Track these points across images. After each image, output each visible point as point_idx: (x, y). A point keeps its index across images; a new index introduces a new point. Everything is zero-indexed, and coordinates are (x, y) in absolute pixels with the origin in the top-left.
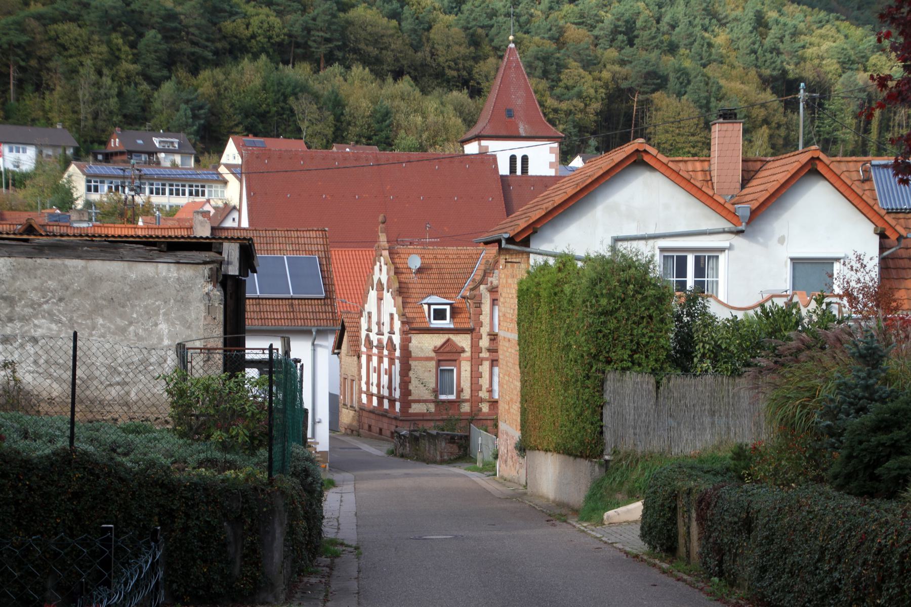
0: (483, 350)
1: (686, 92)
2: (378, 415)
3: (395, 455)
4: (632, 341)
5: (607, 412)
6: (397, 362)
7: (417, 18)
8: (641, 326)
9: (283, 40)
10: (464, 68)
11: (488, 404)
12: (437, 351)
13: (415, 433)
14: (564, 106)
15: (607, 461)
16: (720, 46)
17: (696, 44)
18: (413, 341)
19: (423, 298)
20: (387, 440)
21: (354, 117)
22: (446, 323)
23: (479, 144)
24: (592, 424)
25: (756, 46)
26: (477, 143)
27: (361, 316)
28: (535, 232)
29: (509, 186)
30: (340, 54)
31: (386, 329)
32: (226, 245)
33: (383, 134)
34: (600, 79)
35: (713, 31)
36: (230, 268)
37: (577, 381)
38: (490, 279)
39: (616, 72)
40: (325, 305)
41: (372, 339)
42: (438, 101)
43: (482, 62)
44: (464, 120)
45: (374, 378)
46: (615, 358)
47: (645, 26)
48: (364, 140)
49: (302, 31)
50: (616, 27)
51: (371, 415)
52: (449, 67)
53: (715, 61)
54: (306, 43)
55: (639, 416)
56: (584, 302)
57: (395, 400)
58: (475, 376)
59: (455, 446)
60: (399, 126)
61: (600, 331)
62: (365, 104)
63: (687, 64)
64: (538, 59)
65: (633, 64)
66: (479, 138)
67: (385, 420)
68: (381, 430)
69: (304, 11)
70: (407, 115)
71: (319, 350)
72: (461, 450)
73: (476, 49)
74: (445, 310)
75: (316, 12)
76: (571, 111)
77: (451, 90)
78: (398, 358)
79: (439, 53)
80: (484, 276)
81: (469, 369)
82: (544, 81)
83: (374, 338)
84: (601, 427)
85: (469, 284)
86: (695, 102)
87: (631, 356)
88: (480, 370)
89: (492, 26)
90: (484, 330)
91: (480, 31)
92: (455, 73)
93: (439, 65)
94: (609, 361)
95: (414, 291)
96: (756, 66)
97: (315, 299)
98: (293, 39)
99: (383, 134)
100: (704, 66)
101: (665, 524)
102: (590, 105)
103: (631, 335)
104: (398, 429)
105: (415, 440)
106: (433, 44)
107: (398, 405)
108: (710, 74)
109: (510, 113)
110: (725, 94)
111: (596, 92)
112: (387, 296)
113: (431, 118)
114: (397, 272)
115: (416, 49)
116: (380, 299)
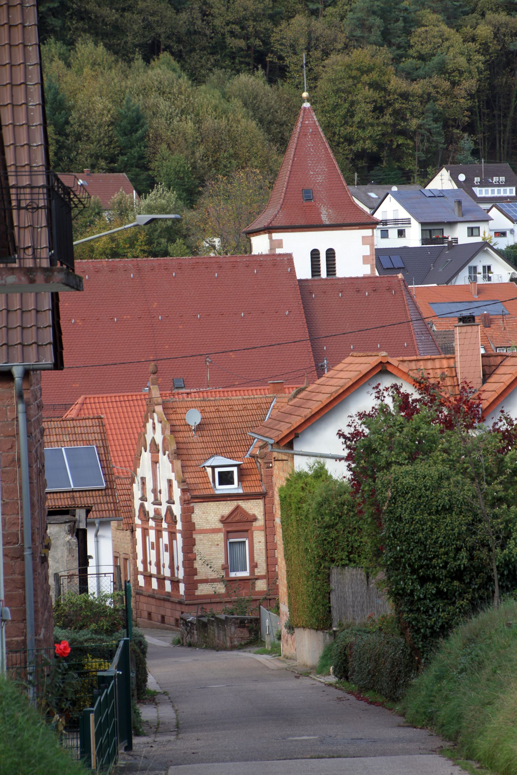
2: (159, 599)
3: (182, 645)
4: (348, 546)
5: (333, 597)
6: (179, 536)
8: (354, 534)
10: (257, 34)
12: (224, 521)
14: (417, 88)
15: (334, 631)
19: (206, 460)
20: (170, 629)
21: (86, 127)
22: (234, 488)
23: (270, 238)
24: (323, 605)
26: (267, 236)
27: (133, 481)
28: (297, 436)
29: (311, 293)
31: (164, 497)
32: (78, 511)
33: (135, 152)
34: (473, 39)
36: (81, 524)
37: (312, 575)
40: (106, 495)
41: (147, 509)
42: (217, 93)
43: (284, 24)
44: (261, 121)
45: (152, 555)
46: (337, 558)
48: (103, 163)
51: (150, 599)
52: (232, 33)
55: (356, 598)
56: (314, 519)
57: (178, 582)
59: (245, 631)
60: (158, 137)
61: (325, 540)
62: (100, 104)
64: (374, 13)
66: (269, 230)
67: (168, 605)
68: (163, 617)
70: (170, 118)
71: (102, 541)
72: (252, 634)
74: (232, 472)
76: (429, 94)
77: (238, 72)
78: (180, 531)
81: (263, 540)
82: (385, 49)
83: (150, 508)
84: (330, 607)
87: (348, 556)
92: (242, 43)
93: (214, 30)
94: (333, 561)
95: (194, 452)
97: (95, 490)
99: (135, 152)
101: (342, 664)
102: (458, 83)
103: (347, 541)
104: (184, 616)
105: (203, 626)
107: (182, 586)
109: (308, 195)
111: (469, 60)
112: (164, 459)
113: (209, 123)
116: (155, 462)
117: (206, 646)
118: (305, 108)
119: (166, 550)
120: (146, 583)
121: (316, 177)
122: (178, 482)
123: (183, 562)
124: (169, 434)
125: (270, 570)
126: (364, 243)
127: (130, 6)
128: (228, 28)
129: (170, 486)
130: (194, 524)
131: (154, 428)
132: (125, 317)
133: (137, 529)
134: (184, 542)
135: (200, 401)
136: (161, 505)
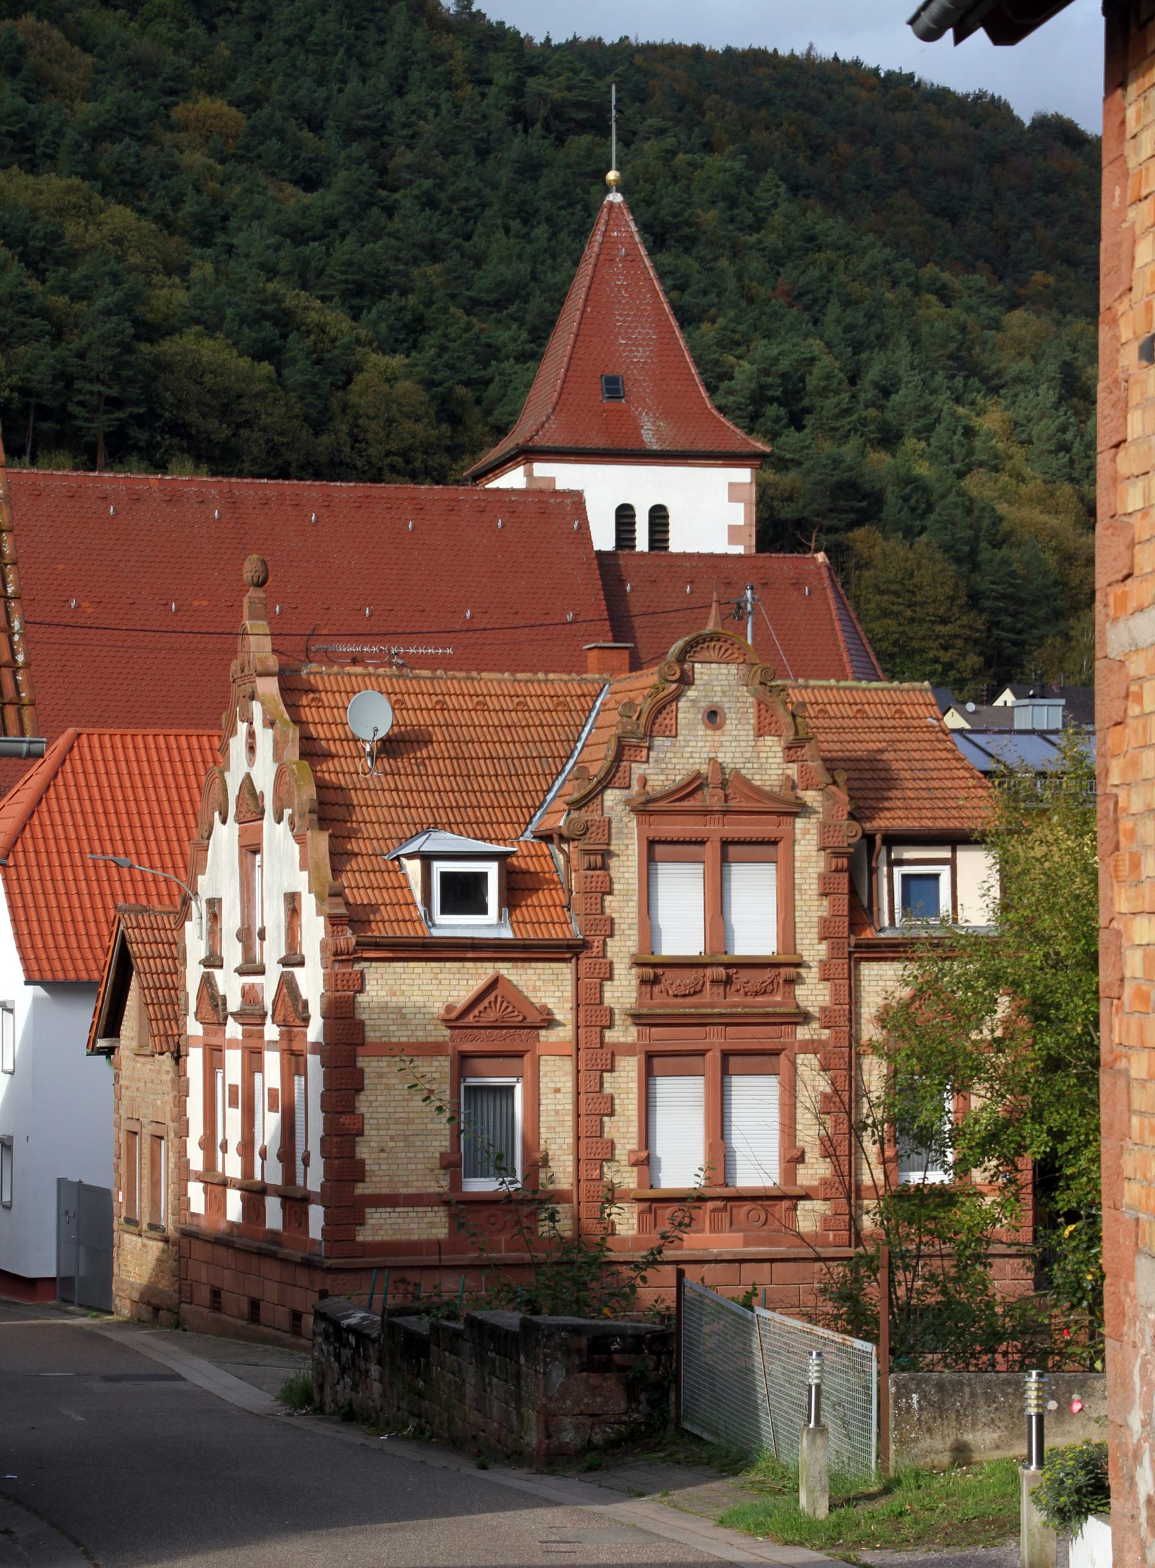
0: (618, 1018)
1: (923, 530)
2: (245, 1251)
3: (320, 1410)
7: (318, 362)
9: (9, 401)
11: (636, 1208)
12: (456, 1020)
13: (411, 1323)
16: (991, 435)
17: (940, 428)
18: (371, 986)
20: (276, 1342)
22: (487, 923)
25: (1069, 436)
27: (185, 915)
29: (622, 583)
30: (140, 435)
31: (272, 951)
35: (973, 403)
38: (638, 769)
39: (768, 485)
45: (231, 1123)
47: (825, 388)
49: (54, 381)
50: (763, 387)
51: (221, 1252)
53: (981, 464)
54: (63, 407)
57: (305, 1199)
58: (593, 1109)
59: (611, 1384)
63: (922, 469)
65: (808, 465)
66: (527, 454)
67: (272, 1269)
68: (255, 1305)
69: (57, 337)
73: (454, 431)
74: (482, 877)
75: (85, 339)
78: (316, 1048)
79: (370, 436)
80: (618, 757)
81: (568, 1084)
83: (230, 985)
85: (564, 787)
86: (947, 548)
88: (608, 1089)
89: (489, 382)
90: (621, 949)
91: (461, 391)
95: (370, 814)
96: (1072, 480)
98: (33, 400)
100: (961, 475)
104: (330, 1305)
105: (407, 1350)
106: (356, 417)
107: (316, 1215)
108: (974, 492)
109: (613, 387)
110: (1011, 533)
112: (278, 837)
114: (311, 751)
115: (318, 428)
116: (251, 849)
117: (420, 1431)
118: (611, 204)
119: (273, 1108)
120: (208, 1205)
121: (631, 351)
122: (319, 897)
123: (322, 1140)
124: (297, 758)
125: (583, 1176)
126: (732, 499)
127: (247, 421)
128: (389, 460)
129: (292, 901)
130: (362, 1023)
131: (252, 749)
132: (196, 603)
133: (192, 1050)
134: (327, 1079)
135: (390, 677)
136: (263, 973)
